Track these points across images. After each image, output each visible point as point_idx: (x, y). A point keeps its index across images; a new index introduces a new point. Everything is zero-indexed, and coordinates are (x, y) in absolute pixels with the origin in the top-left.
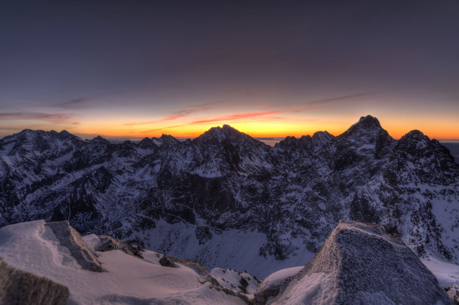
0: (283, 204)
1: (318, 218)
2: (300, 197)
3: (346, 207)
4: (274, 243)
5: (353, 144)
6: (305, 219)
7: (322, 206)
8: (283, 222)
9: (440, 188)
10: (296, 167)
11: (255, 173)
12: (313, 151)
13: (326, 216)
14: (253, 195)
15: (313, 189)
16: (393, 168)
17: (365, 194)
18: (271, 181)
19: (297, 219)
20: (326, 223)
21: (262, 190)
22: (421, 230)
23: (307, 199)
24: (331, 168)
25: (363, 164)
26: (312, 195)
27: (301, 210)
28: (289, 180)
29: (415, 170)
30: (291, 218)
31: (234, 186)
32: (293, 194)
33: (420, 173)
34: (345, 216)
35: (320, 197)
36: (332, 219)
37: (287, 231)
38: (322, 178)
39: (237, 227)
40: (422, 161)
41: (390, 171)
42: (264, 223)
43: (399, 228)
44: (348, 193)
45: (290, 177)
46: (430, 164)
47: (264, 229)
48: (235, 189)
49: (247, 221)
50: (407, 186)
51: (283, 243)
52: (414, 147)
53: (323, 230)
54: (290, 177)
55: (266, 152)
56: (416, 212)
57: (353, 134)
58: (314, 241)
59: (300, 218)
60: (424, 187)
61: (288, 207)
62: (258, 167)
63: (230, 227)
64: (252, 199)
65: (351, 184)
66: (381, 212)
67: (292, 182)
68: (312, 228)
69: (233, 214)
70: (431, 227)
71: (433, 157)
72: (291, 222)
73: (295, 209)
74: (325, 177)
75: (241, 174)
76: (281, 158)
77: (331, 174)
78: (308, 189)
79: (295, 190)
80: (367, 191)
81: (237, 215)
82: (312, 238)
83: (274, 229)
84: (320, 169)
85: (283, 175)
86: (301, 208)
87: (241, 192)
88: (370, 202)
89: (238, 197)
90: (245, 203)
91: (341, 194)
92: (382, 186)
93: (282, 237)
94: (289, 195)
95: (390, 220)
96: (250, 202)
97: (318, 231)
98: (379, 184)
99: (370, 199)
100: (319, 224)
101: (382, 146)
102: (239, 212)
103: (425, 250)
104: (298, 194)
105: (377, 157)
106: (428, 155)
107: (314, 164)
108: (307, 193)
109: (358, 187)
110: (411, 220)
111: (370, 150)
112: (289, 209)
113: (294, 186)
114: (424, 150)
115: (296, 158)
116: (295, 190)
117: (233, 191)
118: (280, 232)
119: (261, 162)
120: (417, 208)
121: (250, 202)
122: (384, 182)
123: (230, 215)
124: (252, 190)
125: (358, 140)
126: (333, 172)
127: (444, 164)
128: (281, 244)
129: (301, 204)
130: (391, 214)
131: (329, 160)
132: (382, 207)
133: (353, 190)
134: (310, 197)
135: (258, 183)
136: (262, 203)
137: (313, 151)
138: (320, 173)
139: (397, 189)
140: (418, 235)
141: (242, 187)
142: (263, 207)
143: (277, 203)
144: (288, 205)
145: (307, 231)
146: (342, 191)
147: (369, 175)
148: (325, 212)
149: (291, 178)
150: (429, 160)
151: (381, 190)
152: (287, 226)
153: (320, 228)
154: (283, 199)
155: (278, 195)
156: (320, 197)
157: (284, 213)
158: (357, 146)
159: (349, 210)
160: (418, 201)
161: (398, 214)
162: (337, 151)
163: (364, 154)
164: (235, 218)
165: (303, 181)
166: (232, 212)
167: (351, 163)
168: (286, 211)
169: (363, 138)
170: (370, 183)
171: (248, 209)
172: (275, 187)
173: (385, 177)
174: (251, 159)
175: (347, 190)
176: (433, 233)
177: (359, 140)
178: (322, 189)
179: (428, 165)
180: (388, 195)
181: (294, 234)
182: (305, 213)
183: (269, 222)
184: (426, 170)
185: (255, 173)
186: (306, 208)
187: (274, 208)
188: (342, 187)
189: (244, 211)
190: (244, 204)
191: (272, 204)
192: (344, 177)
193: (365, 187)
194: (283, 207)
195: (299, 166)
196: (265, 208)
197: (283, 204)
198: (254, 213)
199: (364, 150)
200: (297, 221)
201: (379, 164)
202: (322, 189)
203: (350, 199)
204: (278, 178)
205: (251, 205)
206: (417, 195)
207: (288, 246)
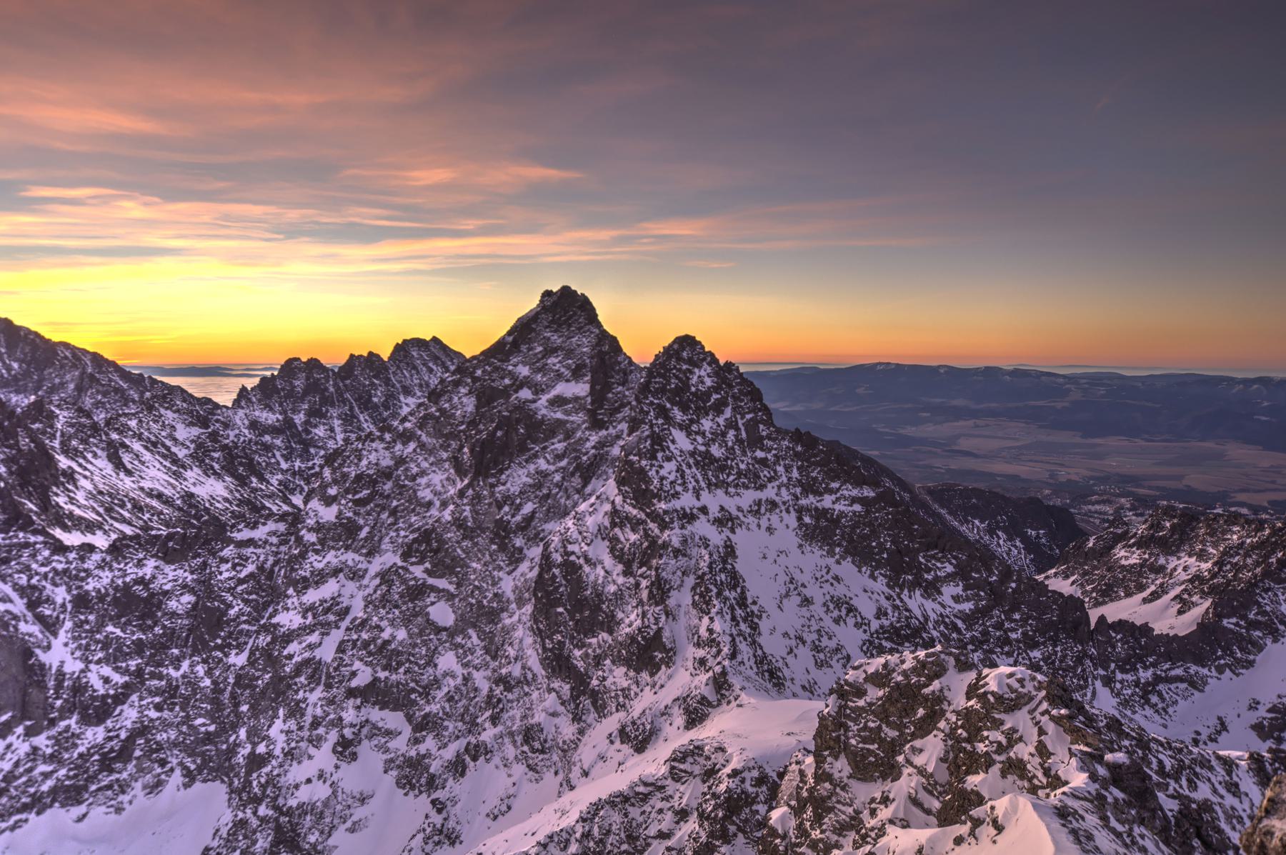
0: (288, 637)
1: (431, 662)
2: (356, 598)
3: (521, 602)
4: (262, 810)
5: (521, 384)
6: (382, 675)
7: (442, 613)
8: (296, 711)
9: (748, 497)
10: (335, 482)
11: (146, 528)
12: (394, 415)
13: (457, 646)
14: (143, 629)
15: (405, 556)
16: (639, 454)
17: (570, 548)
18: (228, 552)
19: (354, 683)
20: (459, 671)
21: (188, 598)
22: (717, 626)
23: (385, 601)
24: (461, 472)
25: (560, 446)
26: (404, 581)
27: (366, 644)
28: (311, 537)
29: (692, 454)
30: (328, 686)
31: (32, 606)
32: (329, 589)
33: (704, 461)
34: (519, 633)
35: (431, 581)
36: (479, 652)
37: (316, 742)
38: (434, 512)
39: (70, 795)
40: (707, 424)
41: (631, 463)
42: (209, 738)
43: (666, 633)
44: (520, 550)
45: (311, 522)
46: (724, 434)
47: (210, 761)
48: (40, 619)
49: (124, 754)
50: (677, 504)
51: (303, 795)
52: (686, 385)
53: (450, 699)
54: (311, 522)
55: (196, 431)
56: (701, 577)
57: (524, 348)
58: (422, 748)
59: (363, 677)
60: (714, 501)
61: (311, 647)
62: (160, 496)
63: (26, 808)
64: (139, 647)
65: (530, 519)
66: (619, 596)
67: (322, 542)
68: (414, 703)
69: (41, 741)
70: (739, 612)
71: (728, 412)
72: (331, 702)
73: (341, 649)
74: (444, 505)
75: (73, 539)
76: (268, 448)
77: (461, 494)
78: (389, 558)
79: (336, 572)
80: (576, 535)
81: (65, 741)
82: (417, 741)
83: (261, 749)
84: (423, 481)
85: (282, 517)
86: (365, 636)
87: (79, 625)
88: (587, 569)
89: (59, 654)
90: (107, 671)
91: (502, 559)
92: (615, 512)
93: (297, 773)
94: (312, 596)
95: (644, 614)
96: (133, 664)
97: (434, 708)
98: (608, 507)
99: (587, 560)
100: (436, 683)
101: (608, 387)
102: (73, 721)
103: (732, 679)
104: (351, 586)
105: (596, 424)
106: (718, 408)
107: (401, 461)
108: (385, 577)
109: (549, 526)
110: (694, 604)
111: (576, 399)
112: (318, 654)
113: (332, 558)
114: (707, 394)
115: (331, 445)
116: (336, 572)
117: (29, 628)
118: (289, 754)
119: (177, 475)
120: (704, 565)
121: (133, 664)
122: (619, 500)
123: (23, 748)
124: (136, 604)
125: (539, 370)
126: (469, 485)
127: (752, 426)
128: (293, 803)
129: (364, 623)
130: (645, 594)
131: (454, 444)
132: (621, 580)
133: (536, 538)
134: (398, 588)
135: (168, 569)
136: (196, 651)
137: (394, 415)
138: (425, 494)
139: (654, 516)
140: (712, 642)
141: (82, 602)
142: (200, 670)
143: (264, 640)
144: (314, 638)
145: (393, 719)
146: (503, 548)
147: (576, 481)
148: (452, 632)
149: (318, 528)
150: (721, 420)
151: (614, 524)
152: (316, 724)
153: (440, 694)
154: (289, 619)
155: (266, 605)
156: (431, 581)
157: (298, 671)
158: (538, 390)
159: (529, 609)
160: (705, 542)
161: (660, 592)
162: (477, 407)
163: (559, 415)
164: (52, 758)
165: (363, 534)
166: (30, 733)
167: (523, 449)
168: (307, 662)
169: (552, 360)
170: (583, 507)
171: (120, 698)
172: (251, 575)
173: (620, 482)
174: (119, 465)
175: (519, 542)
176: (743, 626)
177: (543, 369)
178: (436, 551)
179: (719, 436)
180: (633, 537)
181: (346, 749)
182: (385, 655)
183: (234, 727)
184: (716, 451)
185: (146, 528)
186: (385, 636)
187: (252, 662)
188: (502, 533)
189: (98, 710)
190: (102, 678)
191: (240, 648)
192: (508, 499)
193: (569, 522)
194: (293, 647)
195: (345, 476)
196: (209, 673)
197: (288, 637)
198: (158, 708)
199: (559, 401)
200: (351, 693)
201: (601, 445)
202: (436, 551)
203: (528, 570)
204: (260, 533)
205: (139, 672)
206: (702, 527)
207: (326, 803)
